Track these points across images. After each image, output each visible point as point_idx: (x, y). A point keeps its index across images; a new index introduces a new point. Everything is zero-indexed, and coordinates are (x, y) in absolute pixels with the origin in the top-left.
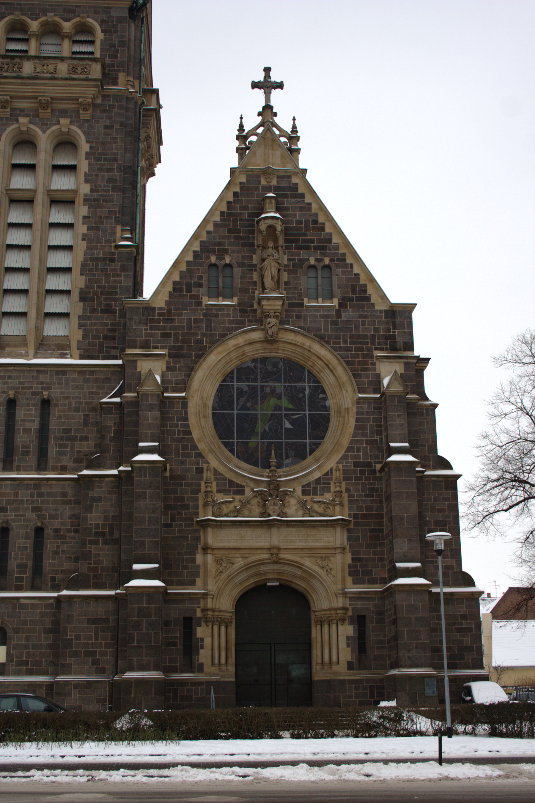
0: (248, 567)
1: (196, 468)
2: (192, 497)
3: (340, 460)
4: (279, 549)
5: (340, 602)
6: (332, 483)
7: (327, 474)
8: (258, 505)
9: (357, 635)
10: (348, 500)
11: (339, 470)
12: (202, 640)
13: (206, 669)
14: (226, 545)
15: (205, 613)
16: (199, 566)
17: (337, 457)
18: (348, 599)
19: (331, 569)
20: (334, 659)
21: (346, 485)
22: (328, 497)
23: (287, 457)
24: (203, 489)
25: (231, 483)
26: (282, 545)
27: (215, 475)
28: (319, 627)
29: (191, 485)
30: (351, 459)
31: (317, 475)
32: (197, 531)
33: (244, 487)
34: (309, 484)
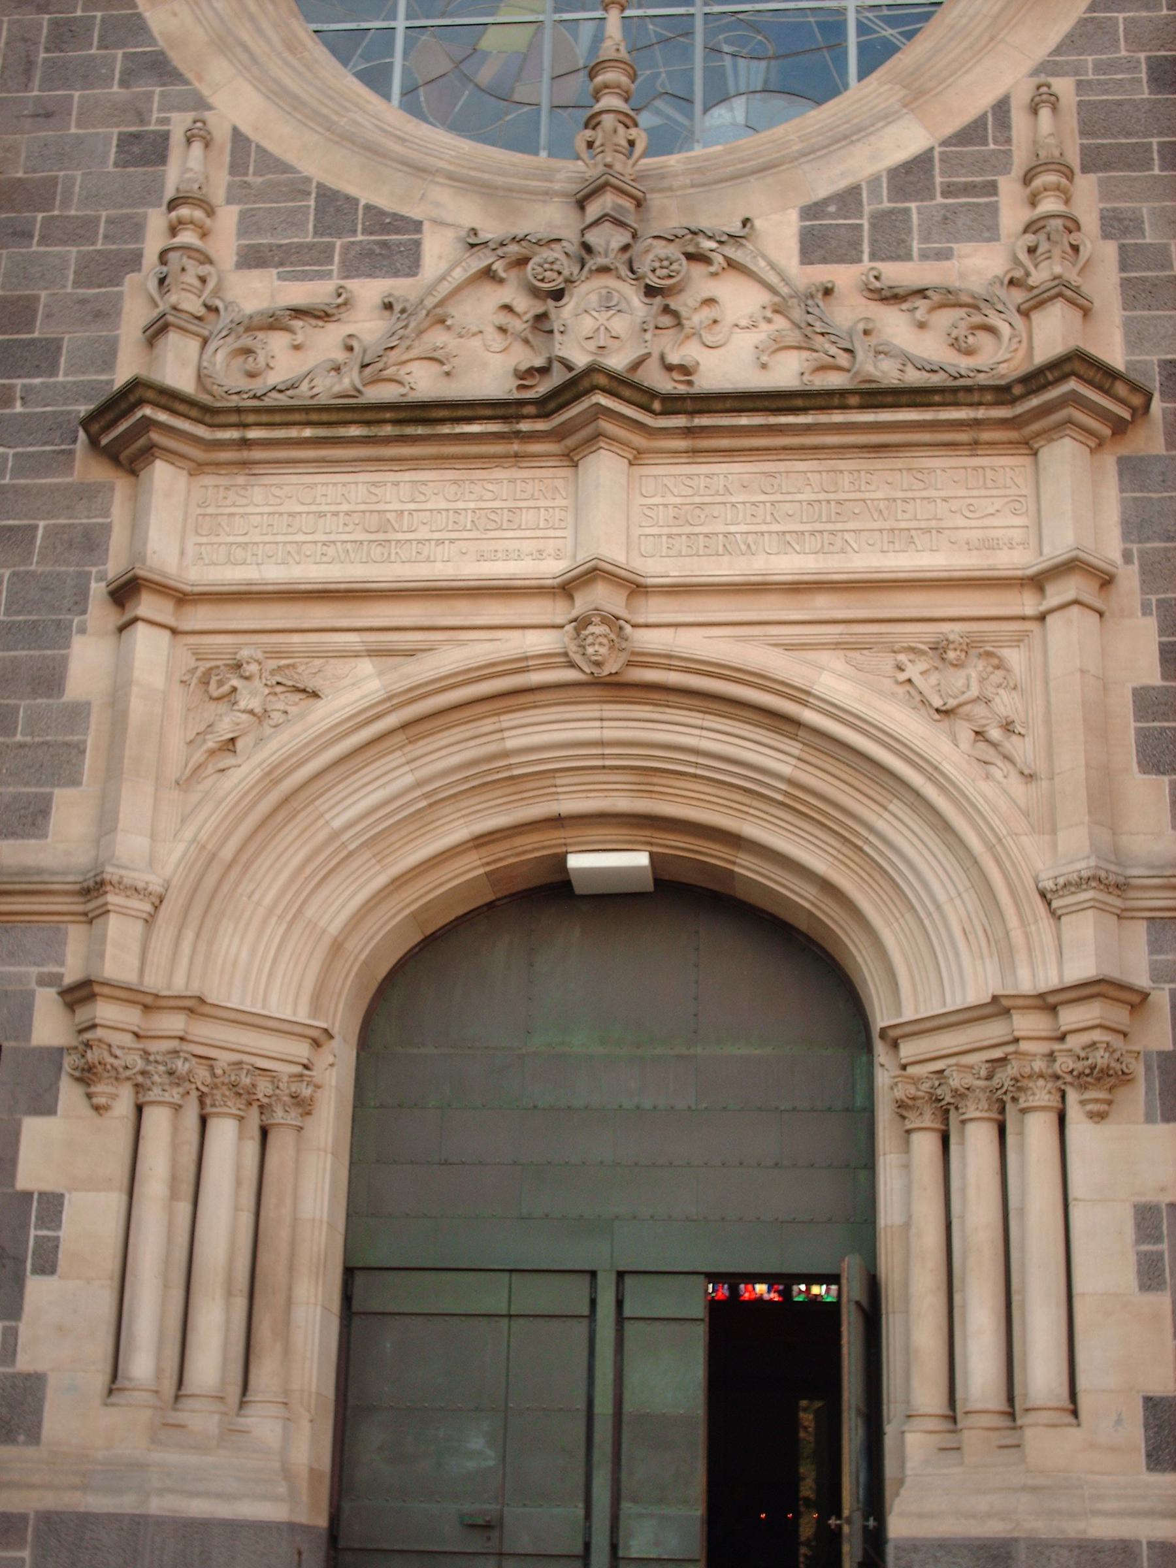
0: (422, 720)
1: (127, 140)
2: (83, 301)
3: (1057, 51)
4: (637, 589)
5: (1081, 949)
6: (1009, 189)
7: (972, 133)
8: (502, 330)
9: (740, 892)
10: (1126, 283)
11: (1054, 104)
12: (52, 1205)
13: (59, 1421)
14: (274, 574)
15: (83, 1014)
16: (78, 713)
17: (1043, 36)
18: (1139, 932)
19: (1008, 727)
20: (1042, 1375)
21: (1106, 192)
22: (979, 264)
23: (719, 96)
24: (154, 241)
25: (334, 208)
26: (656, 567)
27: (237, 167)
28: (925, 1145)
29: (83, 230)
30: (1135, 42)
31: (907, 140)
32: (89, 493)
33: (417, 226)
34: (849, 198)
